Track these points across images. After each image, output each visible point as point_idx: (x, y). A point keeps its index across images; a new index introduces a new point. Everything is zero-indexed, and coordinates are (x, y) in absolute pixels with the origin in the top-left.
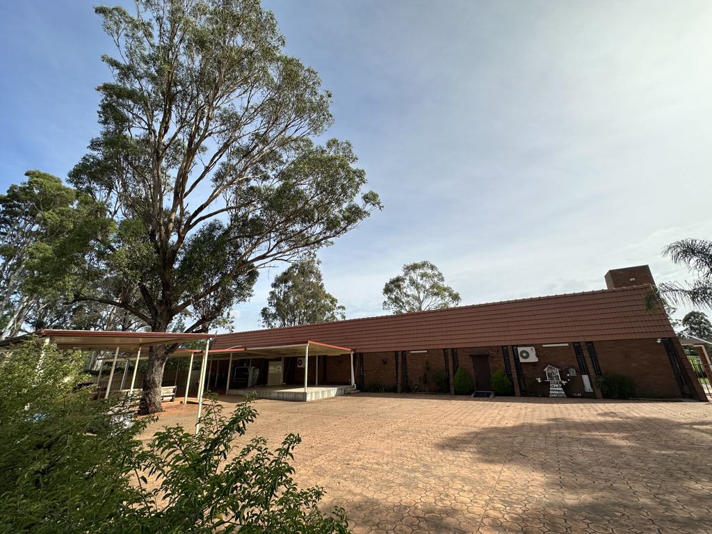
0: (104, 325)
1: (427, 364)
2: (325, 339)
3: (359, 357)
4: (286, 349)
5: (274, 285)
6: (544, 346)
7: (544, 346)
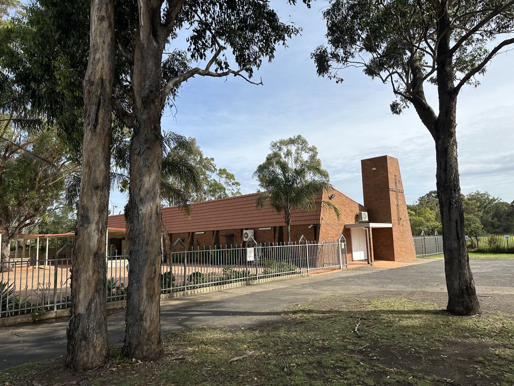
6: (197, 233)
7: (197, 233)
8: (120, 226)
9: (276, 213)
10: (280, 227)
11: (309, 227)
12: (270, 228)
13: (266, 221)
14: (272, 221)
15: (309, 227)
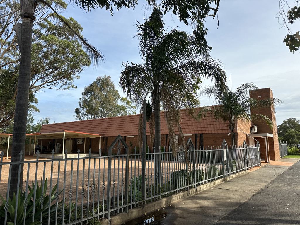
0: (156, 104)
1: (131, 143)
2: (89, 131)
3: (104, 138)
4: (55, 134)
5: (85, 94)
6: (128, 137)
7: (128, 137)
8: (75, 130)
9: (223, 122)
10: (195, 134)
11: (228, 135)
12: (192, 135)
13: (188, 130)
14: (193, 130)
15: (228, 135)
